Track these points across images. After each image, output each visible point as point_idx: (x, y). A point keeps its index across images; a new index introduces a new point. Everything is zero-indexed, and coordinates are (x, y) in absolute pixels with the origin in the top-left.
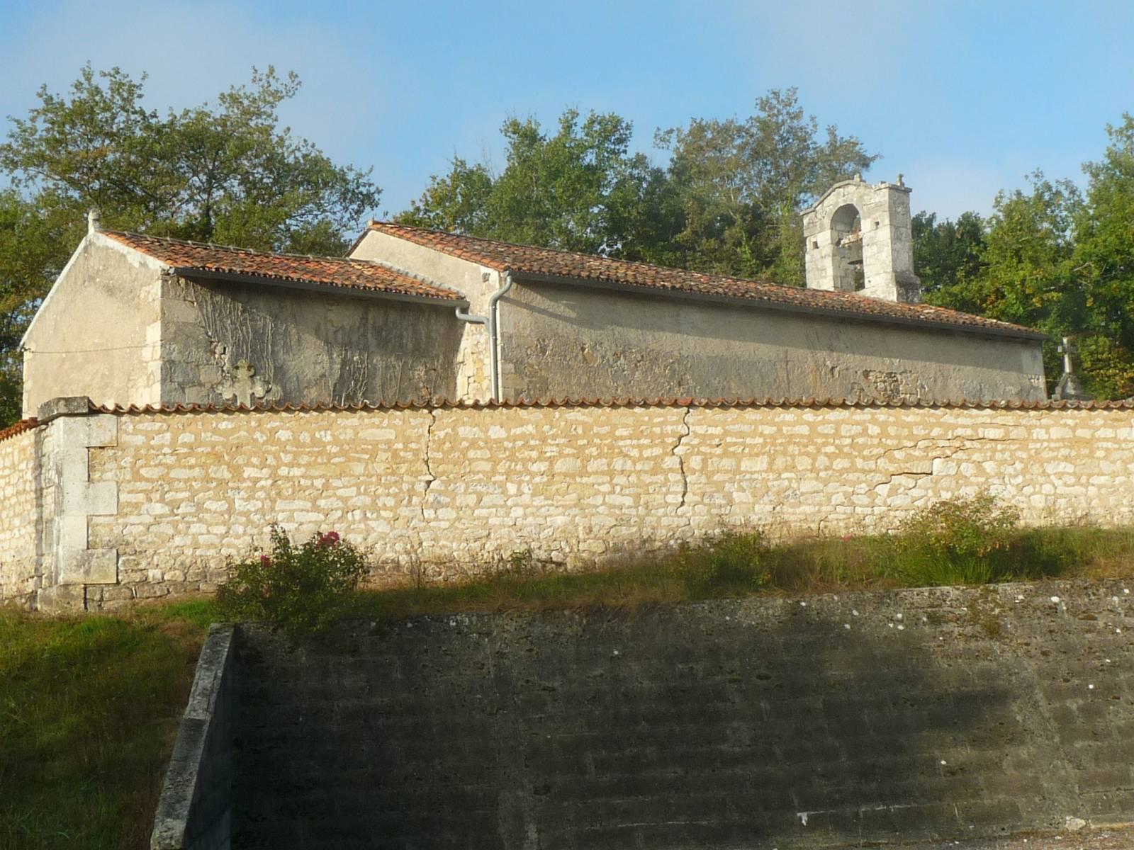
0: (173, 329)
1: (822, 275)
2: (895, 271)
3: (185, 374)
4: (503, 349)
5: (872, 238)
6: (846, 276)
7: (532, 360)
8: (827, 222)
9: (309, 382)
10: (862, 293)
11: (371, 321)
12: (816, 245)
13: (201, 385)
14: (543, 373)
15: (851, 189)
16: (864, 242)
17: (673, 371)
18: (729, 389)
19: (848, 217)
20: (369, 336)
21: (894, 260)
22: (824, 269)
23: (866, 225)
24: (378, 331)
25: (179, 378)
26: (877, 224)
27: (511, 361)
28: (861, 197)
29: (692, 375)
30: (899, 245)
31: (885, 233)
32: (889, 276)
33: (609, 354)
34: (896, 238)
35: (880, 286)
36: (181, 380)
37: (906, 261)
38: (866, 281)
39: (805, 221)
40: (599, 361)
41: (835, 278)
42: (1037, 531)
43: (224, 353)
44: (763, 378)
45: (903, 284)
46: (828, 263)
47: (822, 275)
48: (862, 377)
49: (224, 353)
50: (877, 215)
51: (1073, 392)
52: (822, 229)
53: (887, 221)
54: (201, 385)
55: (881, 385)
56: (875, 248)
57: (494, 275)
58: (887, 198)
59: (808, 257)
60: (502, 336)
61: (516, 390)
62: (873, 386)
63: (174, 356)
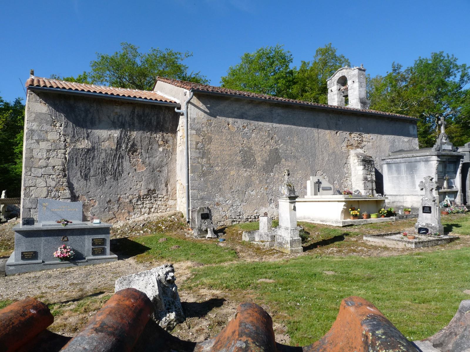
0: (34, 115)
1: (333, 99)
2: (360, 98)
3: (39, 135)
4: (191, 124)
5: (351, 87)
6: (342, 101)
7: (205, 129)
8: (336, 83)
9: (105, 139)
10: (347, 106)
11: (136, 113)
12: (332, 91)
13: (48, 140)
14: (209, 134)
15: (344, 70)
16: (349, 88)
17: (269, 134)
18: (294, 141)
19: (343, 81)
20: (135, 119)
21: (360, 94)
22: (334, 99)
23: (349, 83)
24: (139, 117)
25: (36, 137)
26: (354, 82)
27: (194, 129)
28: (348, 73)
29: (277, 135)
30: (361, 89)
31: (356, 85)
32: (358, 100)
33: (241, 127)
34: (361, 86)
35: (354, 104)
36: (37, 138)
37: (363, 94)
38: (349, 102)
39: (328, 83)
40: (236, 129)
41: (338, 101)
42: (329, 128)
43: (61, 126)
44: (308, 136)
45: (363, 102)
46: (336, 97)
47: (333, 99)
48: (349, 135)
49: (61, 126)
50: (353, 79)
51: (445, 141)
52: (334, 85)
53: (357, 80)
54: (48, 140)
55: (356, 139)
56: (352, 90)
57: (188, 92)
58: (357, 72)
59: (329, 95)
60: (190, 118)
61: (196, 142)
62: (353, 139)
63: (34, 128)
